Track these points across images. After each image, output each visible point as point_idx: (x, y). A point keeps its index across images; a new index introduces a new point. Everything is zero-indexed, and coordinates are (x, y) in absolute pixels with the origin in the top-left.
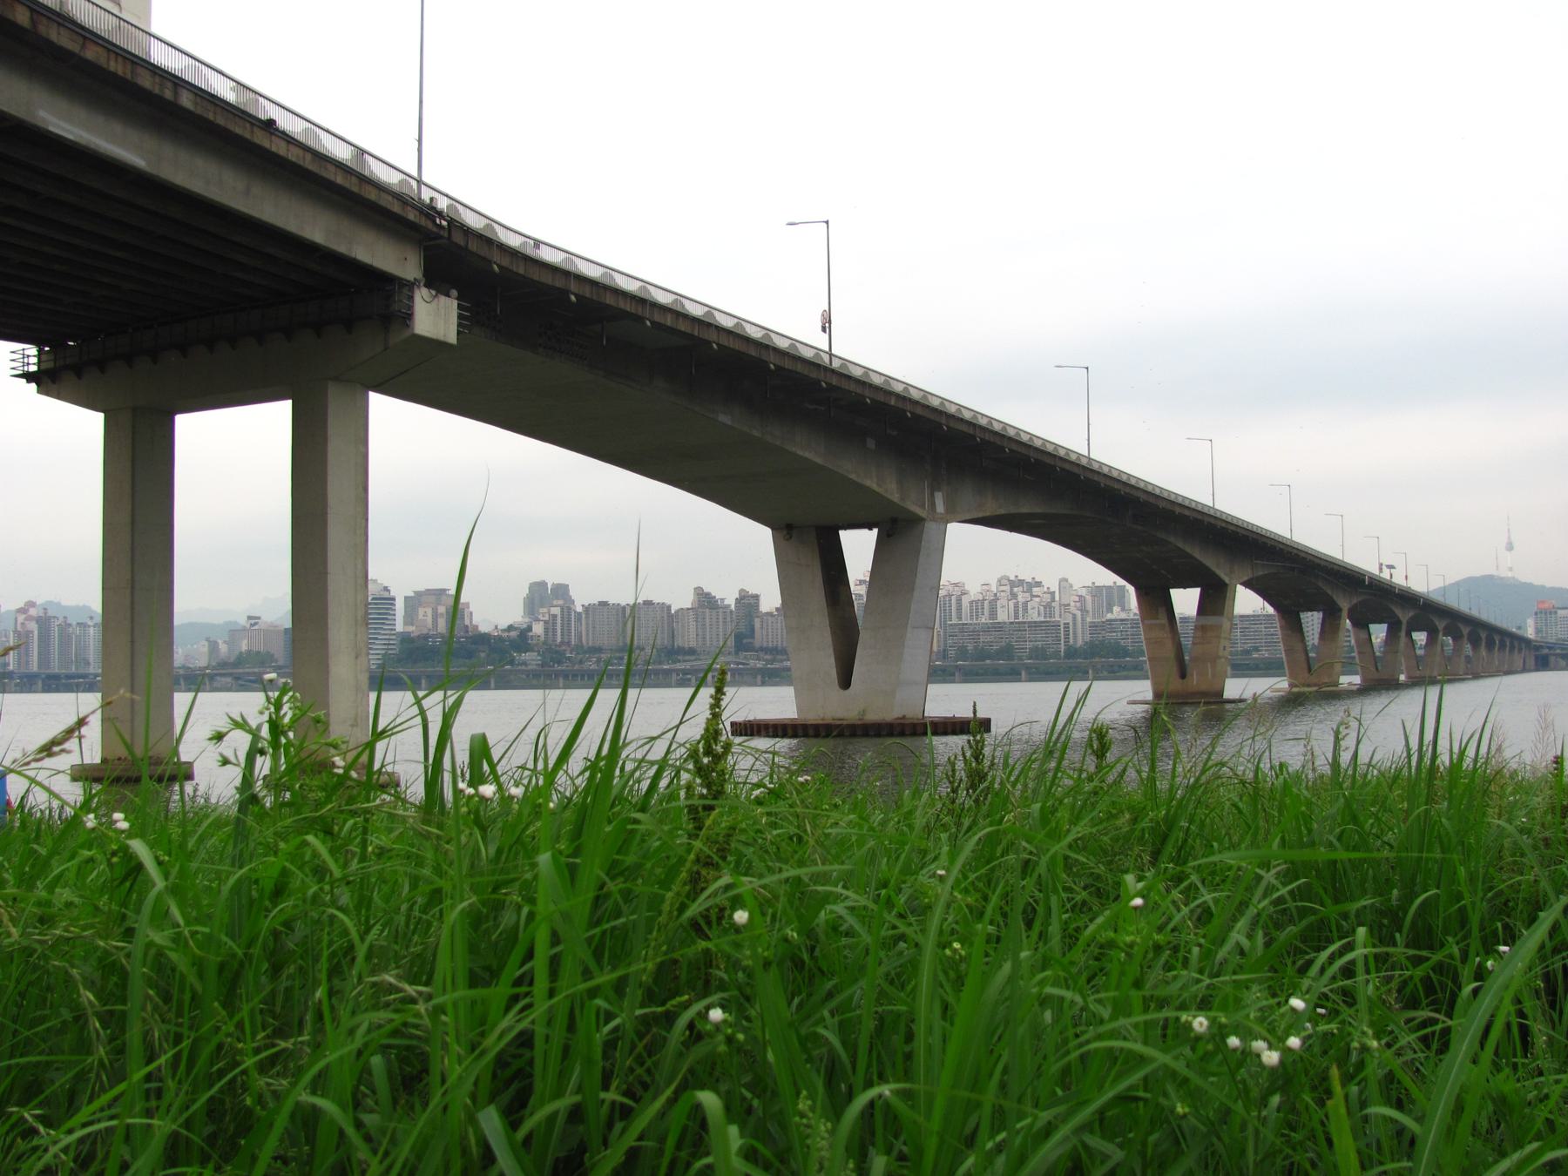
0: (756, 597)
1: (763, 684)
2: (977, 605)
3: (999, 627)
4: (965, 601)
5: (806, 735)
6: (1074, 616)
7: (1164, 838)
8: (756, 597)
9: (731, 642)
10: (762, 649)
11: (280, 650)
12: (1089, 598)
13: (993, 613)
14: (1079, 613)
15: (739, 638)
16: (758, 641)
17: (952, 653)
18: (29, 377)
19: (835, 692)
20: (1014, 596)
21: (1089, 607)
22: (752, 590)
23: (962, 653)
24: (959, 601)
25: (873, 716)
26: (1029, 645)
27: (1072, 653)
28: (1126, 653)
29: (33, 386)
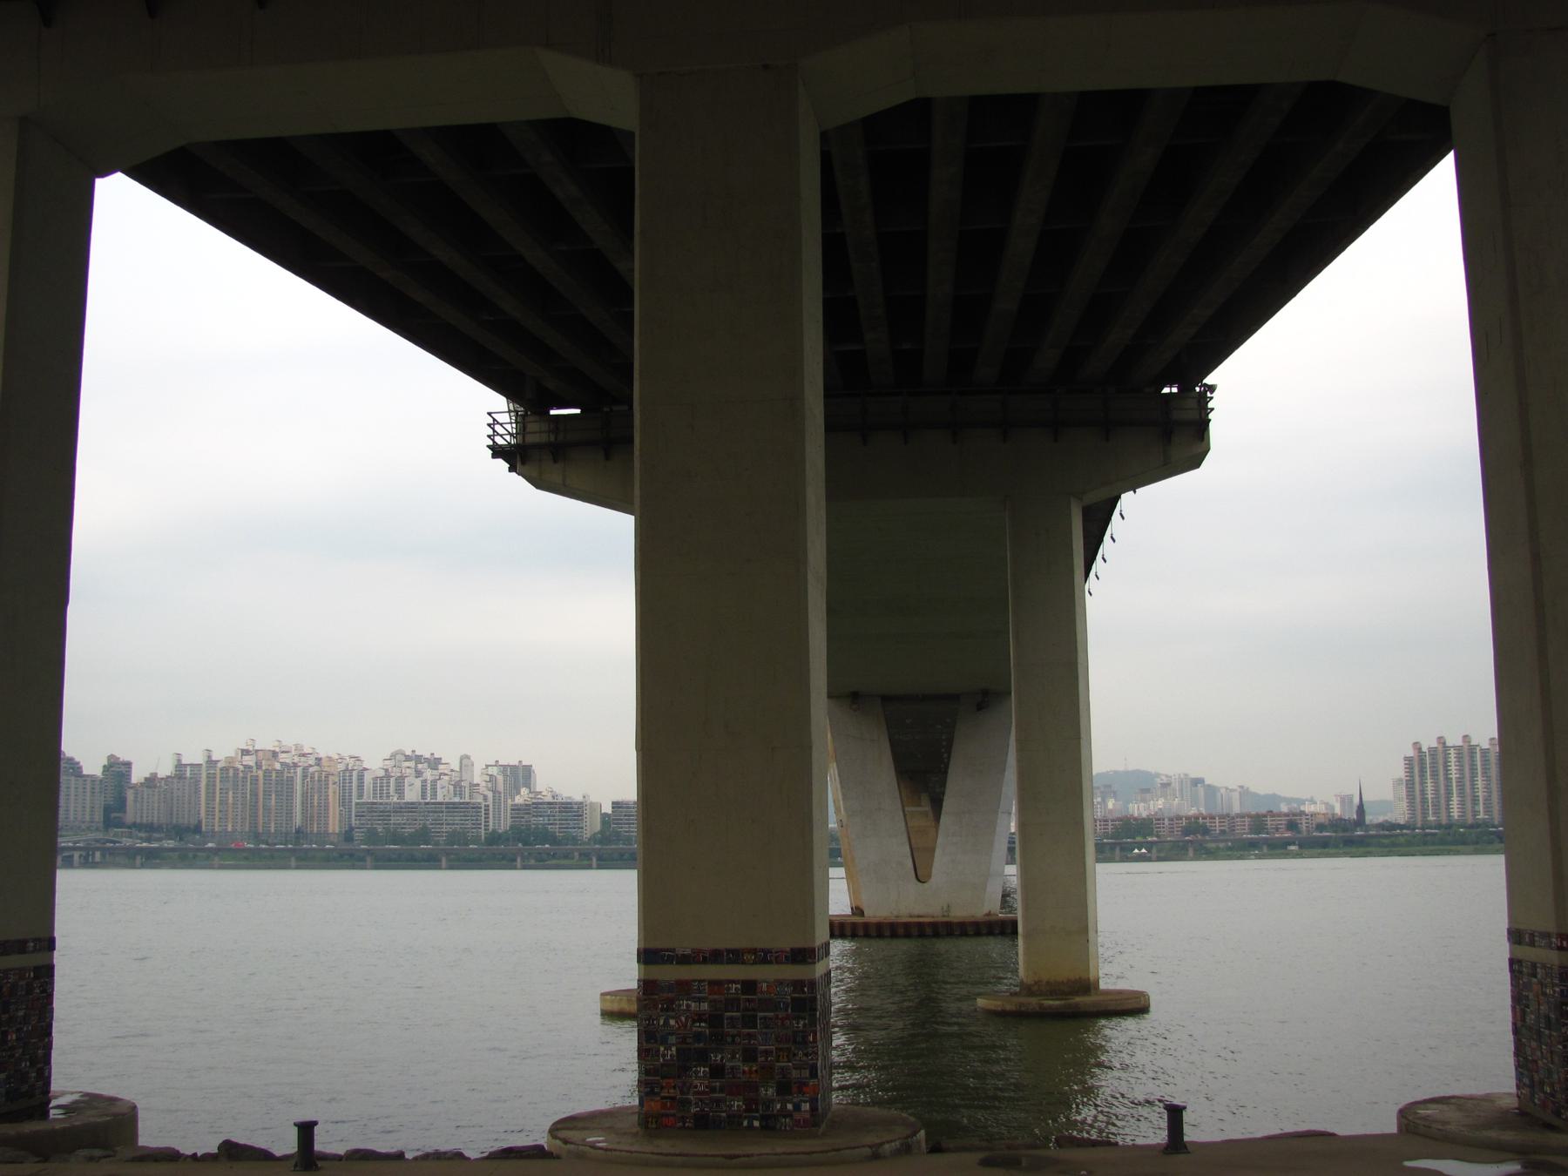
0: (128, 765)
1: (142, 866)
2: (382, 781)
3: (411, 807)
4: (368, 778)
5: (867, 935)
6: (485, 798)
7: (146, 1035)
8: (128, 765)
9: (99, 816)
10: (134, 825)
11: (633, 829)
12: (500, 778)
13: (400, 790)
14: (490, 795)
15: (107, 810)
16: (130, 817)
17: (357, 835)
18: (497, 452)
19: (913, 885)
20: (419, 774)
21: (501, 787)
22: (124, 757)
23: (372, 836)
24: (361, 778)
25: (959, 913)
26: (445, 828)
27: (494, 838)
28: (554, 840)
29: (502, 465)
